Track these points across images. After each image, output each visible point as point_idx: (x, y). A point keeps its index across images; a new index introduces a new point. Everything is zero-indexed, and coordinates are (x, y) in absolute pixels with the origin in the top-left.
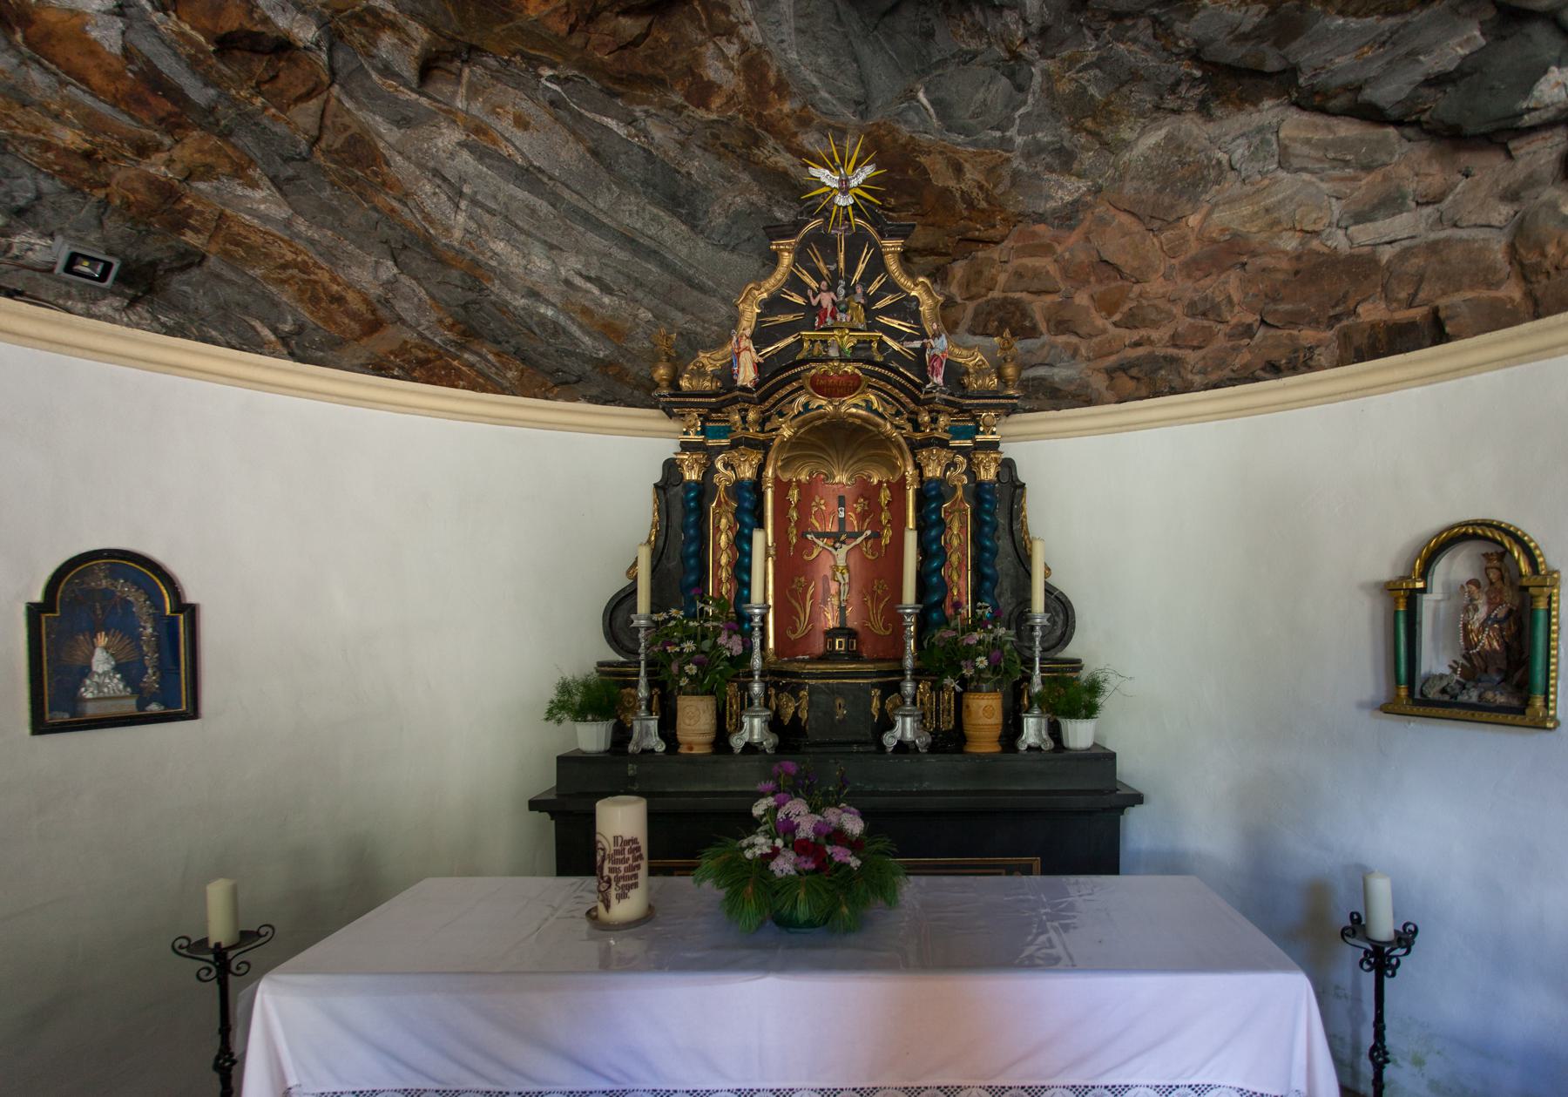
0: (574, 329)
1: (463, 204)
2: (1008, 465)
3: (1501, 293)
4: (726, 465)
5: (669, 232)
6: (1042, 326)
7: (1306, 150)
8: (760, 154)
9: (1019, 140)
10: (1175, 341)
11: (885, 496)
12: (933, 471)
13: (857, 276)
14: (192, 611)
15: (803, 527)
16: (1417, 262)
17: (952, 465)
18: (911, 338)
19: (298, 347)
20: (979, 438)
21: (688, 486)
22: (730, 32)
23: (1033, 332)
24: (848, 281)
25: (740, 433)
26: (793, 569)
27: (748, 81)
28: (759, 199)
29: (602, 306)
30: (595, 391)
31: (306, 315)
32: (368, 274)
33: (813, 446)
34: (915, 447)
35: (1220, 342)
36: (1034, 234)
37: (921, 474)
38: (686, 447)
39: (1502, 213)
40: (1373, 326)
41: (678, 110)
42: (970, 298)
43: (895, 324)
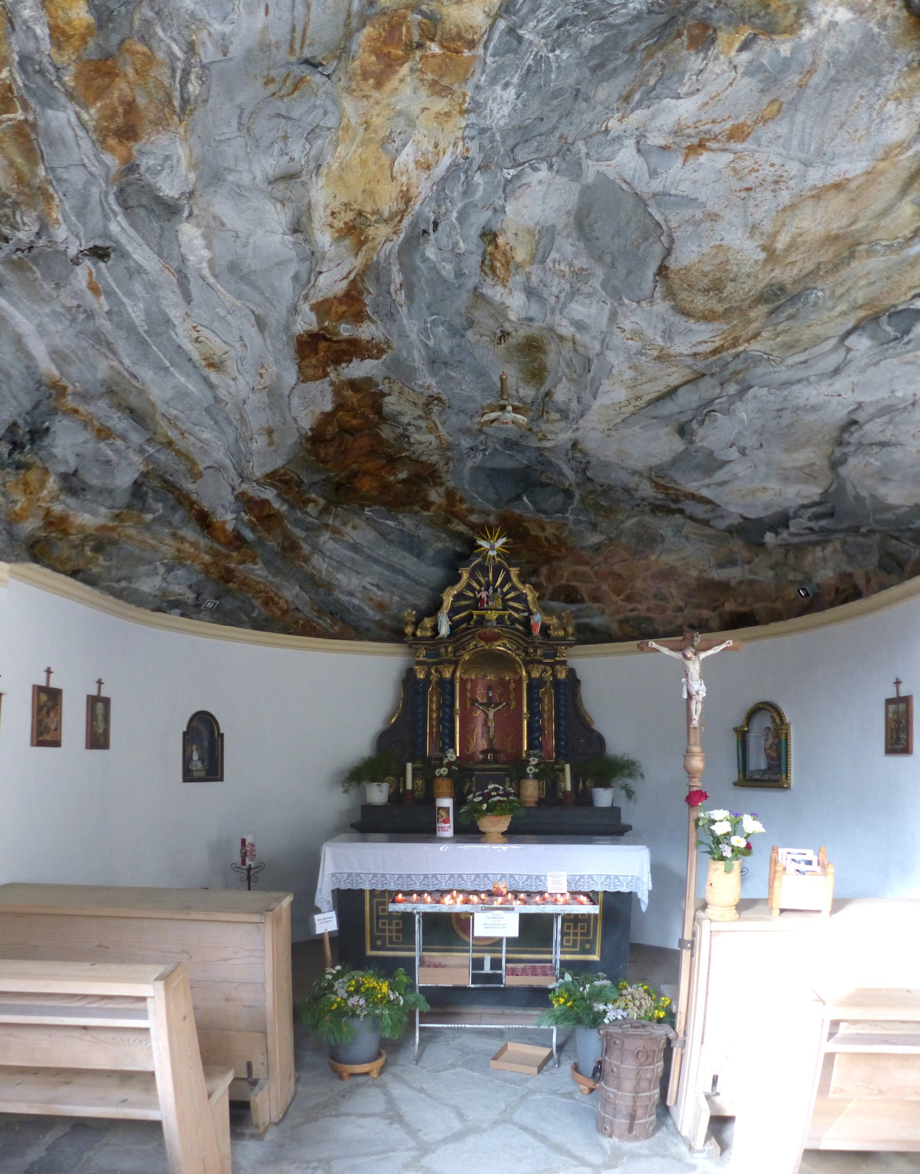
2: (572, 672)
5: (409, 562)
6: (586, 598)
8: (450, 526)
9: (571, 518)
10: (649, 609)
11: (512, 686)
12: (535, 674)
13: (498, 583)
14: (221, 736)
17: (545, 671)
18: (523, 611)
19: (259, 625)
22: (441, 484)
23: (582, 601)
34: (526, 663)
35: (670, 613)
38: (419, 663)
39: (771, 573)
40: (731, 612)
43: (516, 605)
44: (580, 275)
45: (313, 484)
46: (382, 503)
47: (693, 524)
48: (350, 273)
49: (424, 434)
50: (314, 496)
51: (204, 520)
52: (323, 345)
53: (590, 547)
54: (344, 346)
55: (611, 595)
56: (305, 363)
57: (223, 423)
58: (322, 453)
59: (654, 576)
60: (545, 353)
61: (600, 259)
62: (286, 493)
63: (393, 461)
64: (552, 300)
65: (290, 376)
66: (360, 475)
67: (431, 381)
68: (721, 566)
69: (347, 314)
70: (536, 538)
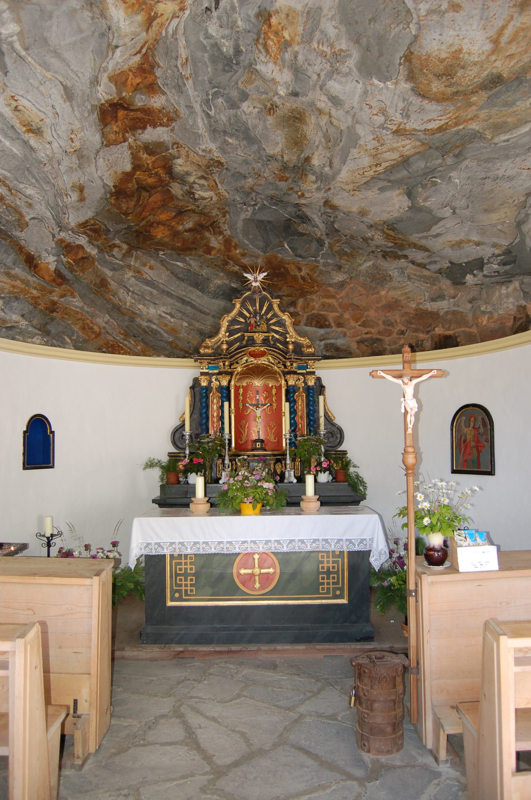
0: (162, 332)
1: (130, 294)
2: (319, 379)
3: (471, 330)
4: (216, 380)
5: (195, 296)
6: (333, 324)
7: (415, 277)
9: (322, 261)
11: (274, 391)
12: (291, 382)
13: (263, 312)
15: (244, 401)
16: (449, 317)
19: (79, 346)
20: (308, 370)
21: (202, 388)
22: (221, 233)
23: (329, 326)
24: (260, 313)
25: (222, 370)
26: (241, 417)
27: (225, 247)
28: (227, 282)
29: (171, 322)
30: (167, 352)
32: (102, 320)
33: (248, 374)
35: (395, 335)
36: (329, 291)
37: (287, 384)
38: (202, 374)
39: (469, 306)
41: (200, 256)
42: (306, 313)
44: (338, 57)
45: (117, 232)
46: (173, 249)
47: (414, 267)
48: (142, 48)
49: (206, 190)
50: (117, 242)
51: (31, 262)
52: (121, 113)
53: (336, 283)
54: (139, 115)
55: (351, 321)
56: (108, 129)
58: (124, 206)
60: (305, 123)
61: (357, 42)
62: (96, 240)
63: (181, 213)
64: (315, 77)
65: (94, 137)
66: (155, 225)
67: (212, 146)
68: (433, 300)
69: (141, 85)
70: (295, 277)
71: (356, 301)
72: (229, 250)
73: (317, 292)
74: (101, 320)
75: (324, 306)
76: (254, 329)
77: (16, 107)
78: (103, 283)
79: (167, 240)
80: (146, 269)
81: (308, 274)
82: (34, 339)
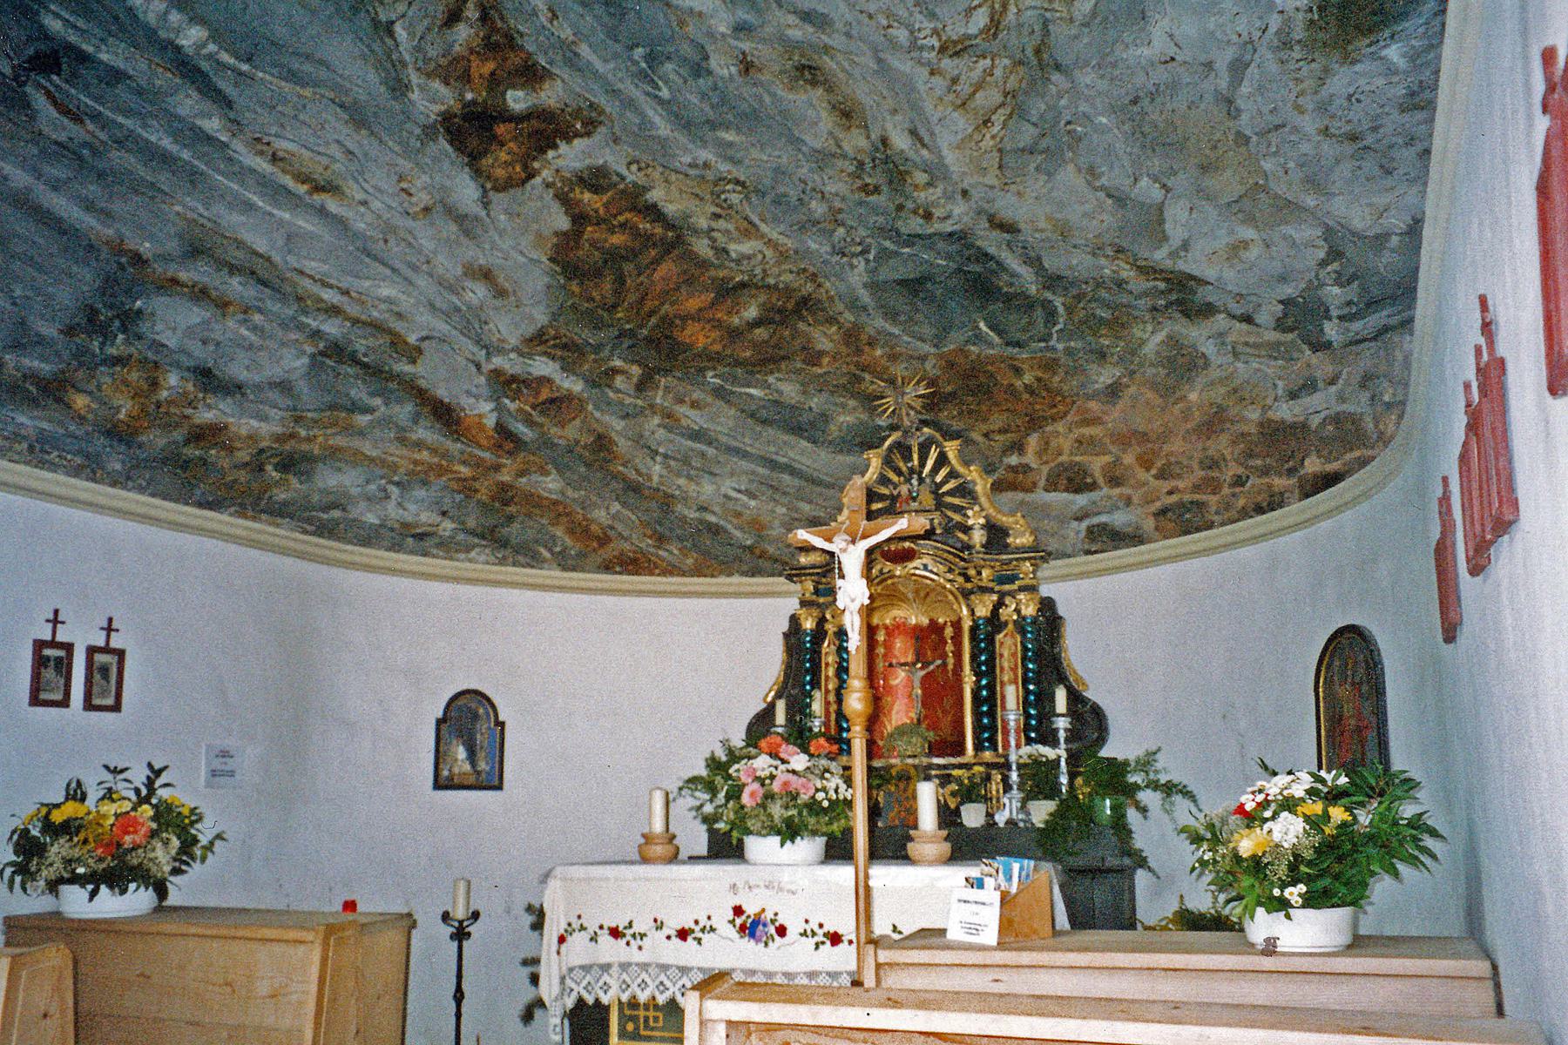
2: (1047, 605)
6: (1101, 481)
9: (1060, 346)
11: (949, 632)
23: (1093, 487)
30: (745, 568)
31: (569, 542)
34: (966, 594)
35: (1226, 491)
36: (1087, 410)
39: (1365, 396)
40: (1315, 476)
42: (1046, 463)
43: (956, 501)
50: (618, 363)
51: (445, 415)
57: (409, 273)
59: (1197, 430)
63: (729, 292)
71: (1140, 424)
72: (859, 352)
73: (1065, 414)
74: (603, 513)
75: (1080, 443)
76: (905, 507)
77: (274, 154)
78: (602, 443)
79: (717, 347)
80: (682, 410)
81: (1039, 380)
82: (473, 554)
